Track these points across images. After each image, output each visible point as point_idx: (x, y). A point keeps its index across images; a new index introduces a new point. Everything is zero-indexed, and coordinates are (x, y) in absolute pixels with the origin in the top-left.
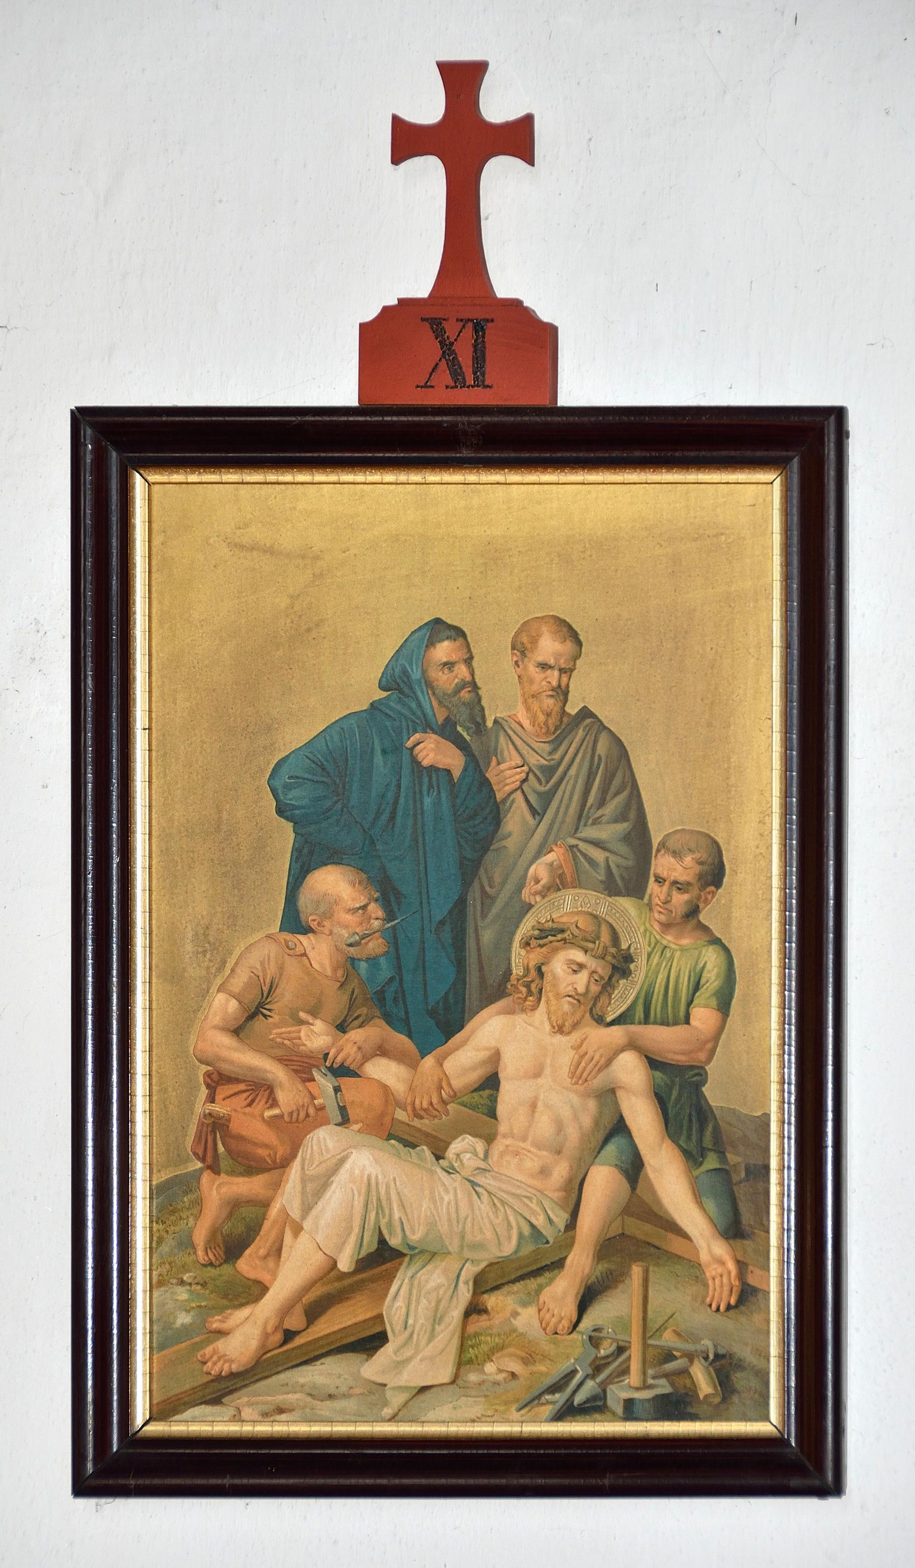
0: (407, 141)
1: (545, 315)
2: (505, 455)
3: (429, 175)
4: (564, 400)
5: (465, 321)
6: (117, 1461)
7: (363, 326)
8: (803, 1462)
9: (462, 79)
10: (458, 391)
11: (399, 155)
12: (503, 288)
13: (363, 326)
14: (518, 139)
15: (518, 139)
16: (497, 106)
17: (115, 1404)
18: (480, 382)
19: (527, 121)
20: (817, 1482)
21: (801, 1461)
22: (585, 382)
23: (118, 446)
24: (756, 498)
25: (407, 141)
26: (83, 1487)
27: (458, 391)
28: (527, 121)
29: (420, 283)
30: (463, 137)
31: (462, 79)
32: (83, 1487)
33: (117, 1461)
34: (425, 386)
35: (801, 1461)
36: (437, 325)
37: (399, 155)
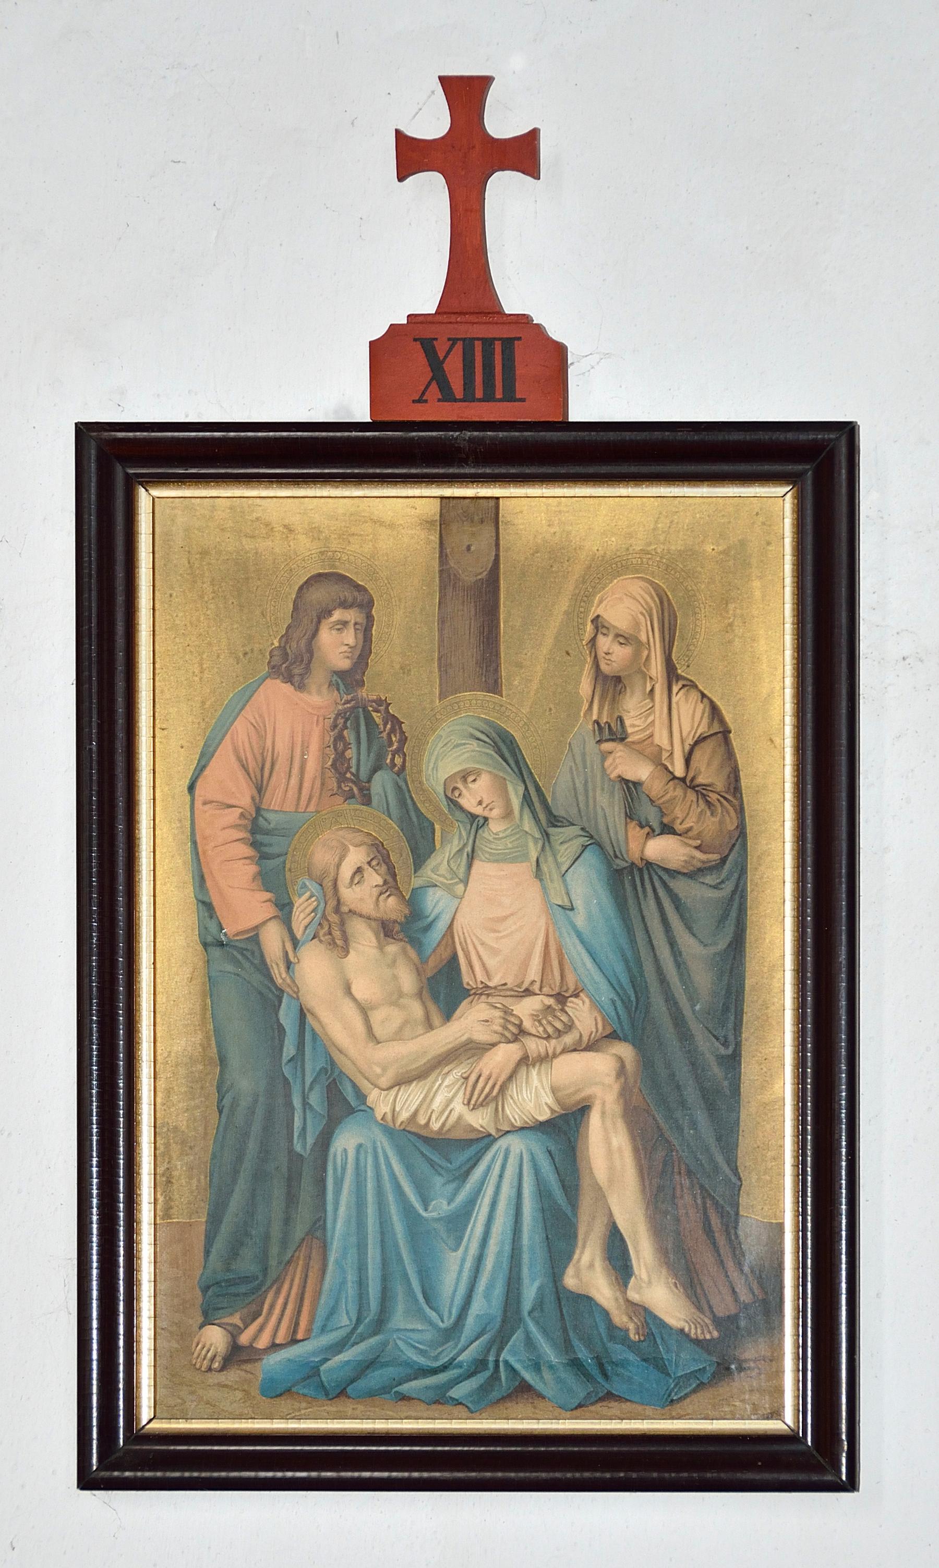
0: (411, 156)
1: (555, 333)
2: (497, 471)
3: (431, 191)
4: (576, 414)
5: (454, 341)
6: (120, 1454)
7: (372, 344)
8: (817, 1458)
9: (467, 94)
10: (469, 406)
11: (530, 140)
12: (511, 304)
13: (372, 344)
14: (523, 154)
15: (523, 154)
16: (501, 123)
17: (95, 1382)
18: (510, 396)
19: (532, 136)
20: (829, 1478)
21: (815, 1457)
22: (594, 399)
23: (118, 464)
24: (772, 508)
25: (411, 156)
26: (87, 1481)
27: (469, 406)
28: (532, 136)
29: (426, 299)
30: (467, 151)
31: (467, 94)
32: (87, 1481)
33: (120, 1454)
34: (419, 401)
35: (815, 1457)
36: (428, 346)
37: (530, 140)
